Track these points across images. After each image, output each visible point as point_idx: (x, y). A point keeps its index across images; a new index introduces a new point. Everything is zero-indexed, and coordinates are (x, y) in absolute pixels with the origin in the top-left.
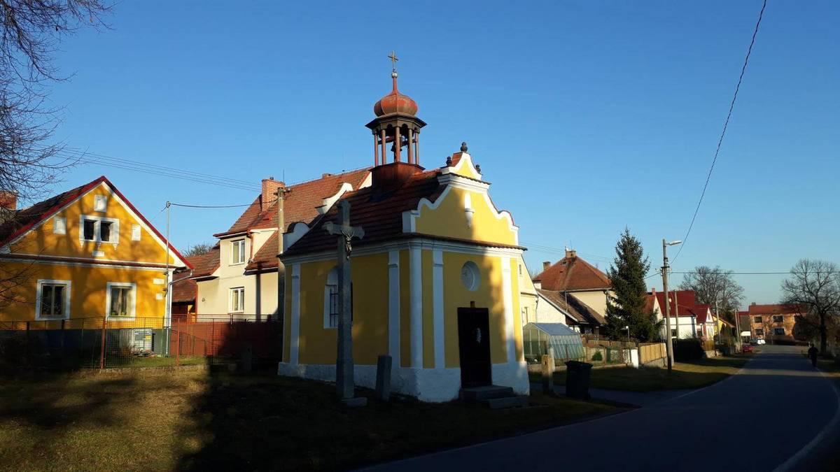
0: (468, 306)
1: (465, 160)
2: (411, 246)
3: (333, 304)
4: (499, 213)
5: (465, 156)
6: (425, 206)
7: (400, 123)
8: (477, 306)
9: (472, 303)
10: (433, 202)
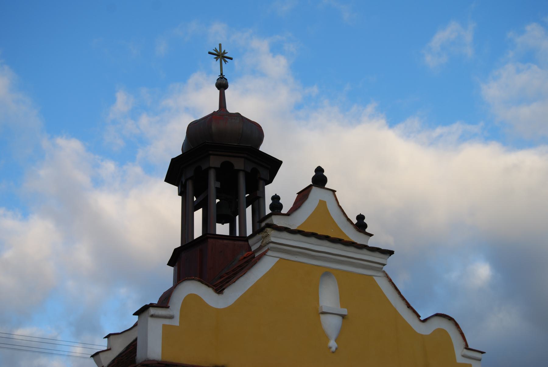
7: (215, 162)
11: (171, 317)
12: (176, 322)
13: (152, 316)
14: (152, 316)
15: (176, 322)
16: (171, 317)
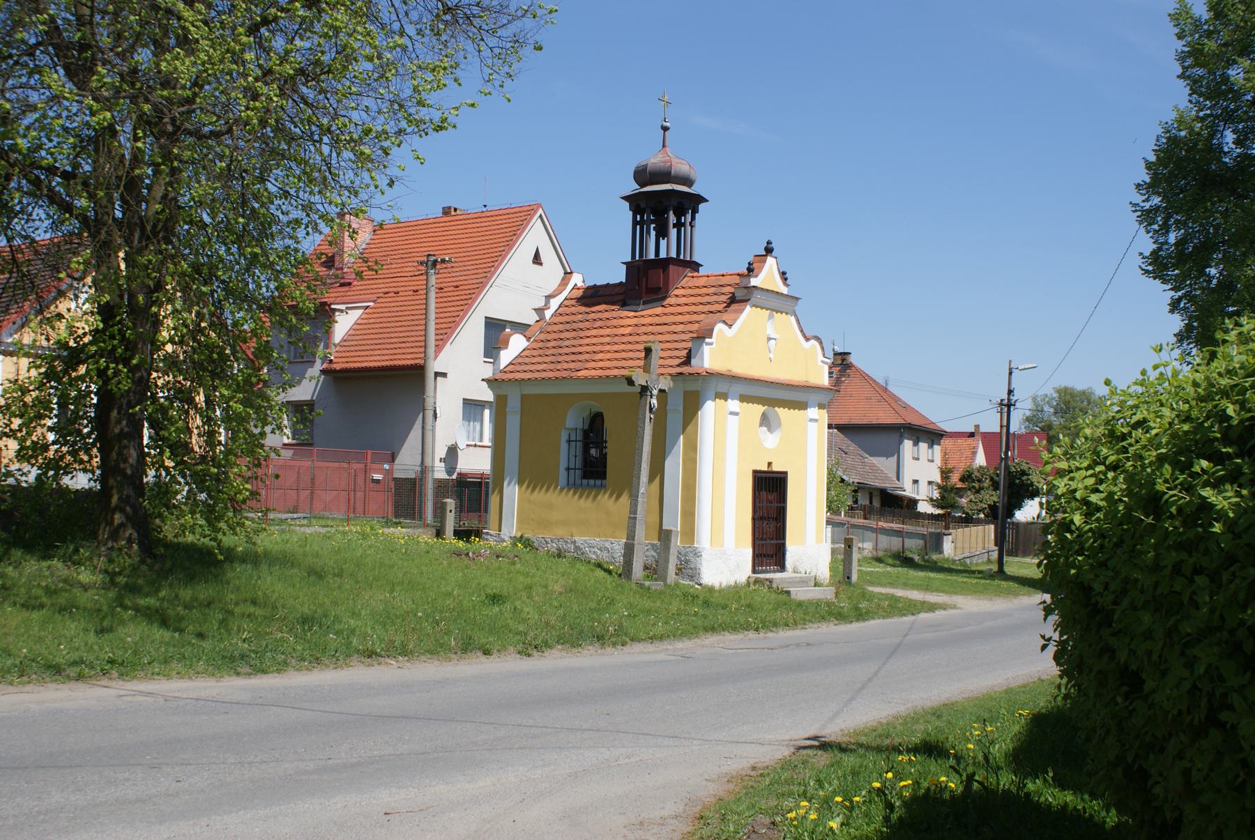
0: (765, 468)
1: (771, 265)
3: (572, 452)
4: (807, 339)
5: (770, 261)
6: (721, 331)
8: (775, 468)
9: (770, 464)
10: (730, 326)
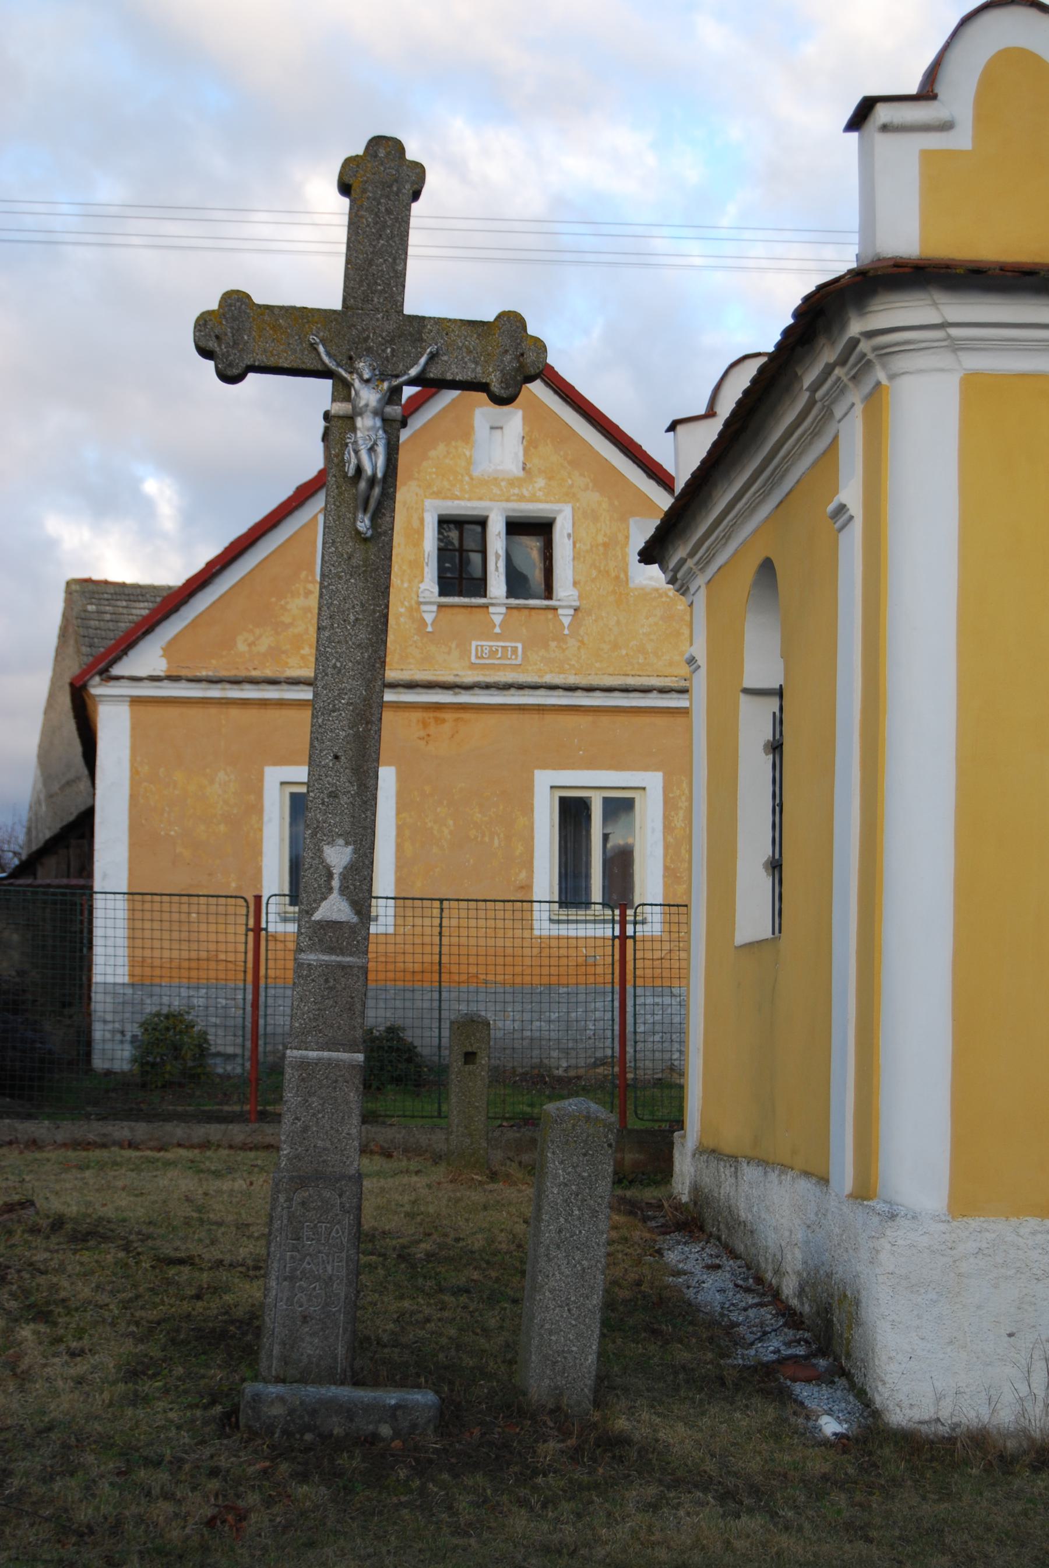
2: (885, 353)
11: (946, 126)
12: (962, 139)
13: (885, 128)
14: (885, 128)
15: (962, 139)
16: (946, 126)
